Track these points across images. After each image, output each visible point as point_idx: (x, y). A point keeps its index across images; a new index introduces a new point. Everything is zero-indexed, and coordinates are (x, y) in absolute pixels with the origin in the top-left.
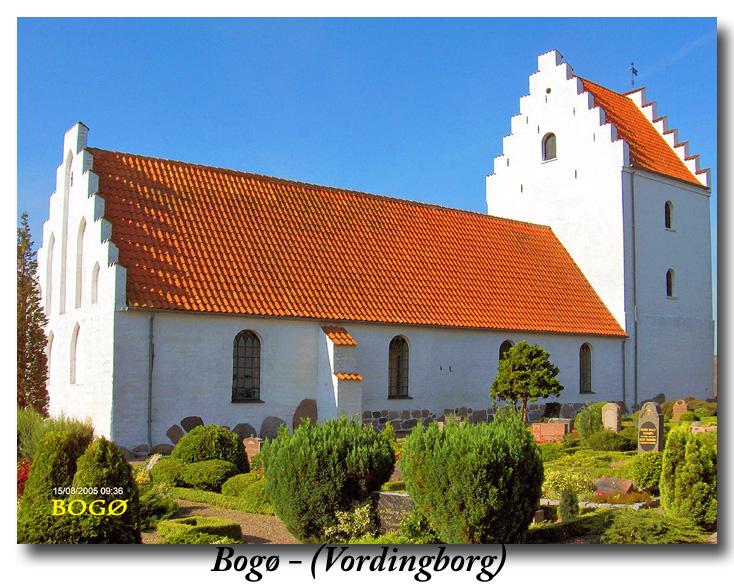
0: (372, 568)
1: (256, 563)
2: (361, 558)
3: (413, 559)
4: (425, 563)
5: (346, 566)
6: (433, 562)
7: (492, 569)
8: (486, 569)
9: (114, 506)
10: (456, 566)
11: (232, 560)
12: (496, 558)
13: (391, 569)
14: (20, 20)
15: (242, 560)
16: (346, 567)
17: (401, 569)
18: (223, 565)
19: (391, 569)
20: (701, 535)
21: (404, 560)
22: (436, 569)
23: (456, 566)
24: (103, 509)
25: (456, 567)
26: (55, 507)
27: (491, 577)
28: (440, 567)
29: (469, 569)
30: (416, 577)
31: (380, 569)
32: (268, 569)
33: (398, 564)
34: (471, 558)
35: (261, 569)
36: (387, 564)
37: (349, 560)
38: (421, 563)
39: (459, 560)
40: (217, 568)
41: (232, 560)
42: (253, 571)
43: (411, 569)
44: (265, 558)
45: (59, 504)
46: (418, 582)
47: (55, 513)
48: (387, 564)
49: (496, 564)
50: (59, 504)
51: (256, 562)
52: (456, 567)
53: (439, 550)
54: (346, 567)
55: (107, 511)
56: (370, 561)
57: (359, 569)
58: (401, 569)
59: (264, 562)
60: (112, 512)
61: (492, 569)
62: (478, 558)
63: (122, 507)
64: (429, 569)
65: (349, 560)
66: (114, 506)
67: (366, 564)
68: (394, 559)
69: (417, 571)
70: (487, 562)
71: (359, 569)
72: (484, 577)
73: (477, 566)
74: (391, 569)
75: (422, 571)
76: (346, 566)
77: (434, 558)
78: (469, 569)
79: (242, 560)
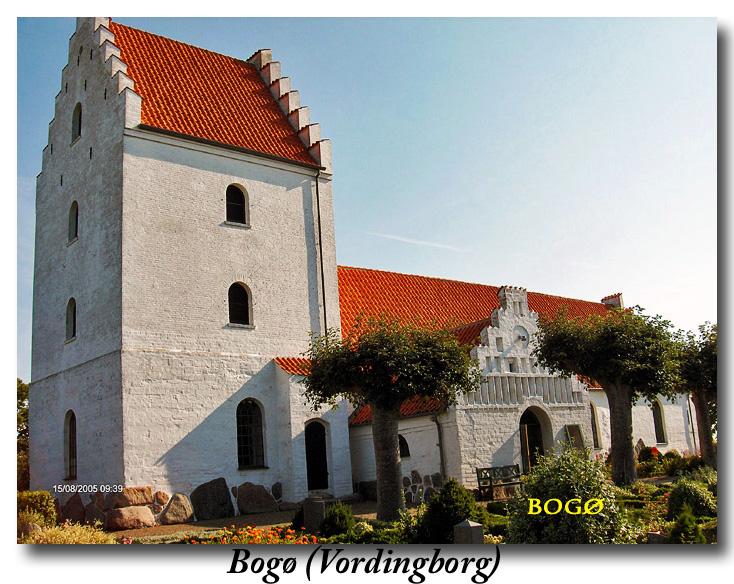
0: (367, 570)
1: (273, 565)
2: (356, 560)
3: (407, 561)
4: (419, 565)
5: (341, 568)
6: (428, 564)
7: (487, 571)
8: (272, 571)
9: (591, 504)
10: (450, 568)
11: (249, 562)
12: (491, 560)
13: (386, 571)
14: (21, 21)
15: (259, 562)
16: (341, 569)
17: (395, 571)
18: (239, 566)
19: (386, 571)
20: (687, 527)
21: (399, 561)
22: (431, 571)
23: (450, 568)
24: (579, 508)
25: (450, 569)
26: (531, 506)
27: (486, 578)
28: (434, 569)
29: (464, 571)
30: (410, 579)
31: (376, 571)
32: (285, 571)
33: (392, 566)
34: (466, 560)
35: (278, 571)
36: (382, 566)
37: (344, 562)
38: (415, 565)
39: (453, 562)
40: (233, 570)
41: (249, 562)
42: (270, 573)
43: (405, 571)
44: (282, 560)
45: (535, 503)
46: (409, 582)
47: (531, 512)
48: (382, 566)
49: (491, 565)
50: (535, 503)
51: (273, 564)
52: (450, 569)
53: (434, 552)
54: (341, 569)
55: (583, 510)
56: (365, 563)
57: (354, 571)
58: (395, 571)
59: (281, 564)
60: (587, 511)
61: (487, 571)
62: (473, 560)
63: (598, 508)
64: (424, 571)
65: (344, 562)
66: (591, 504)
67: (362, 566)
68: (389, 561)
69: (411, 573)
70: (482, 564)
71: (354, 571)
72: (480, 579)
73: (472, 568)
74: (386, 571)
75: (416, 573)
76: (341, 568)
77: (428, 560)
78: (464, 571)
79: (259, 562)
